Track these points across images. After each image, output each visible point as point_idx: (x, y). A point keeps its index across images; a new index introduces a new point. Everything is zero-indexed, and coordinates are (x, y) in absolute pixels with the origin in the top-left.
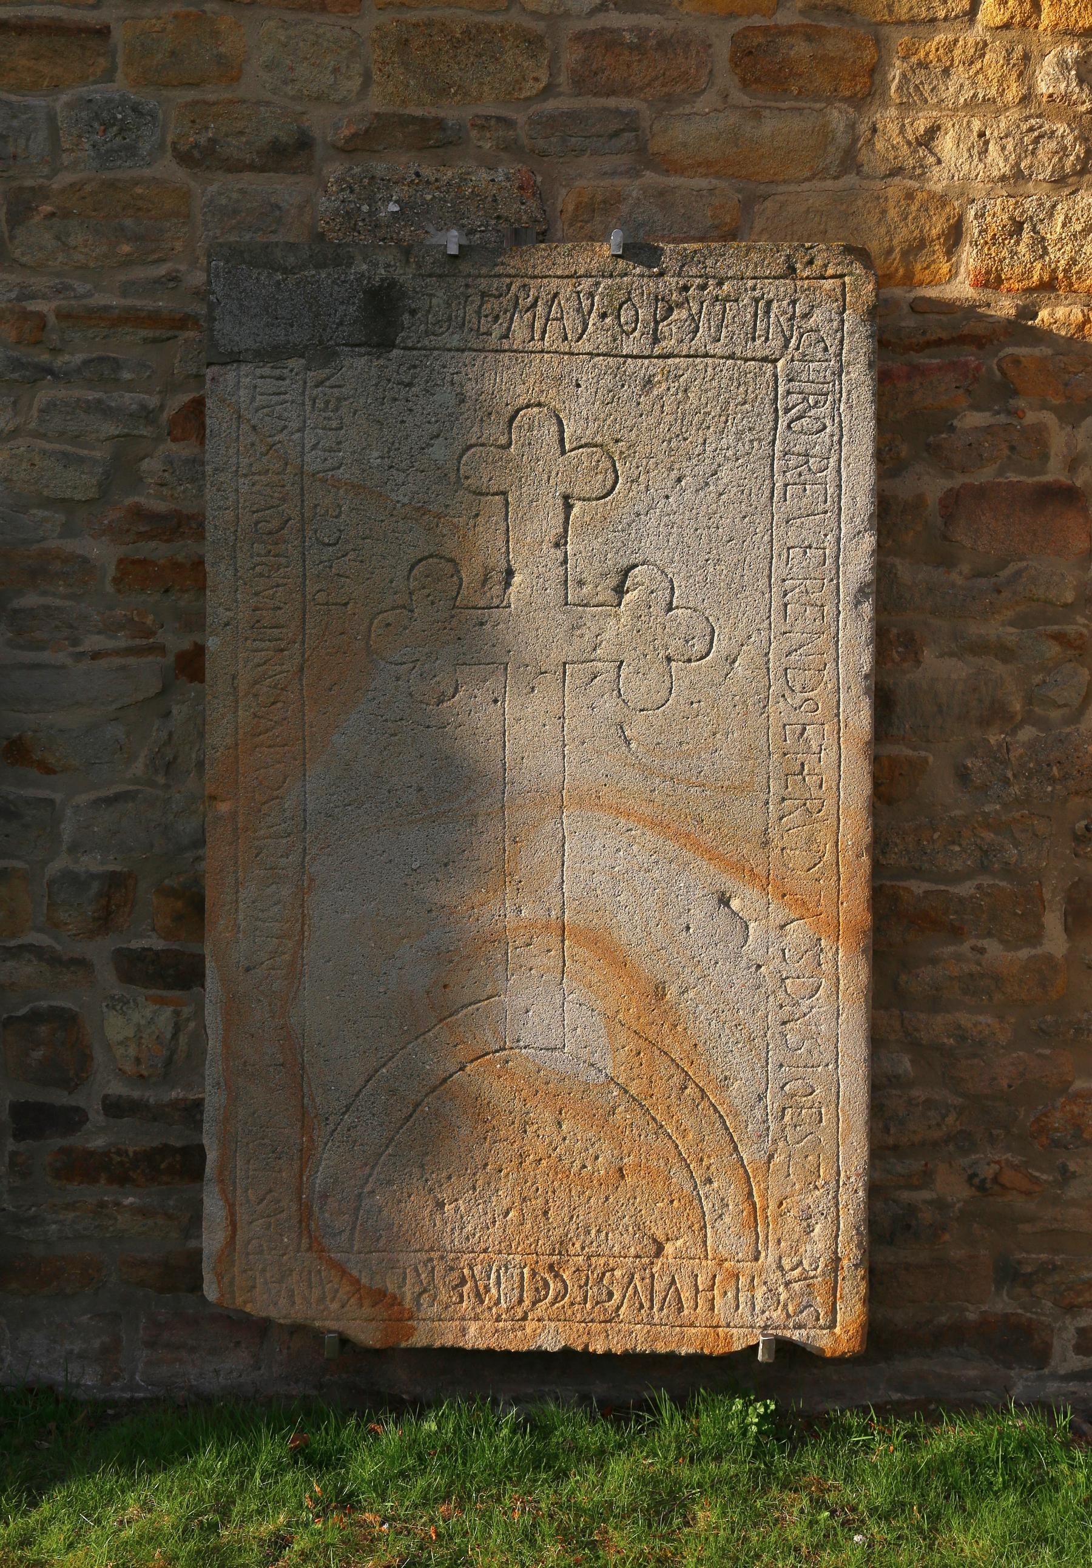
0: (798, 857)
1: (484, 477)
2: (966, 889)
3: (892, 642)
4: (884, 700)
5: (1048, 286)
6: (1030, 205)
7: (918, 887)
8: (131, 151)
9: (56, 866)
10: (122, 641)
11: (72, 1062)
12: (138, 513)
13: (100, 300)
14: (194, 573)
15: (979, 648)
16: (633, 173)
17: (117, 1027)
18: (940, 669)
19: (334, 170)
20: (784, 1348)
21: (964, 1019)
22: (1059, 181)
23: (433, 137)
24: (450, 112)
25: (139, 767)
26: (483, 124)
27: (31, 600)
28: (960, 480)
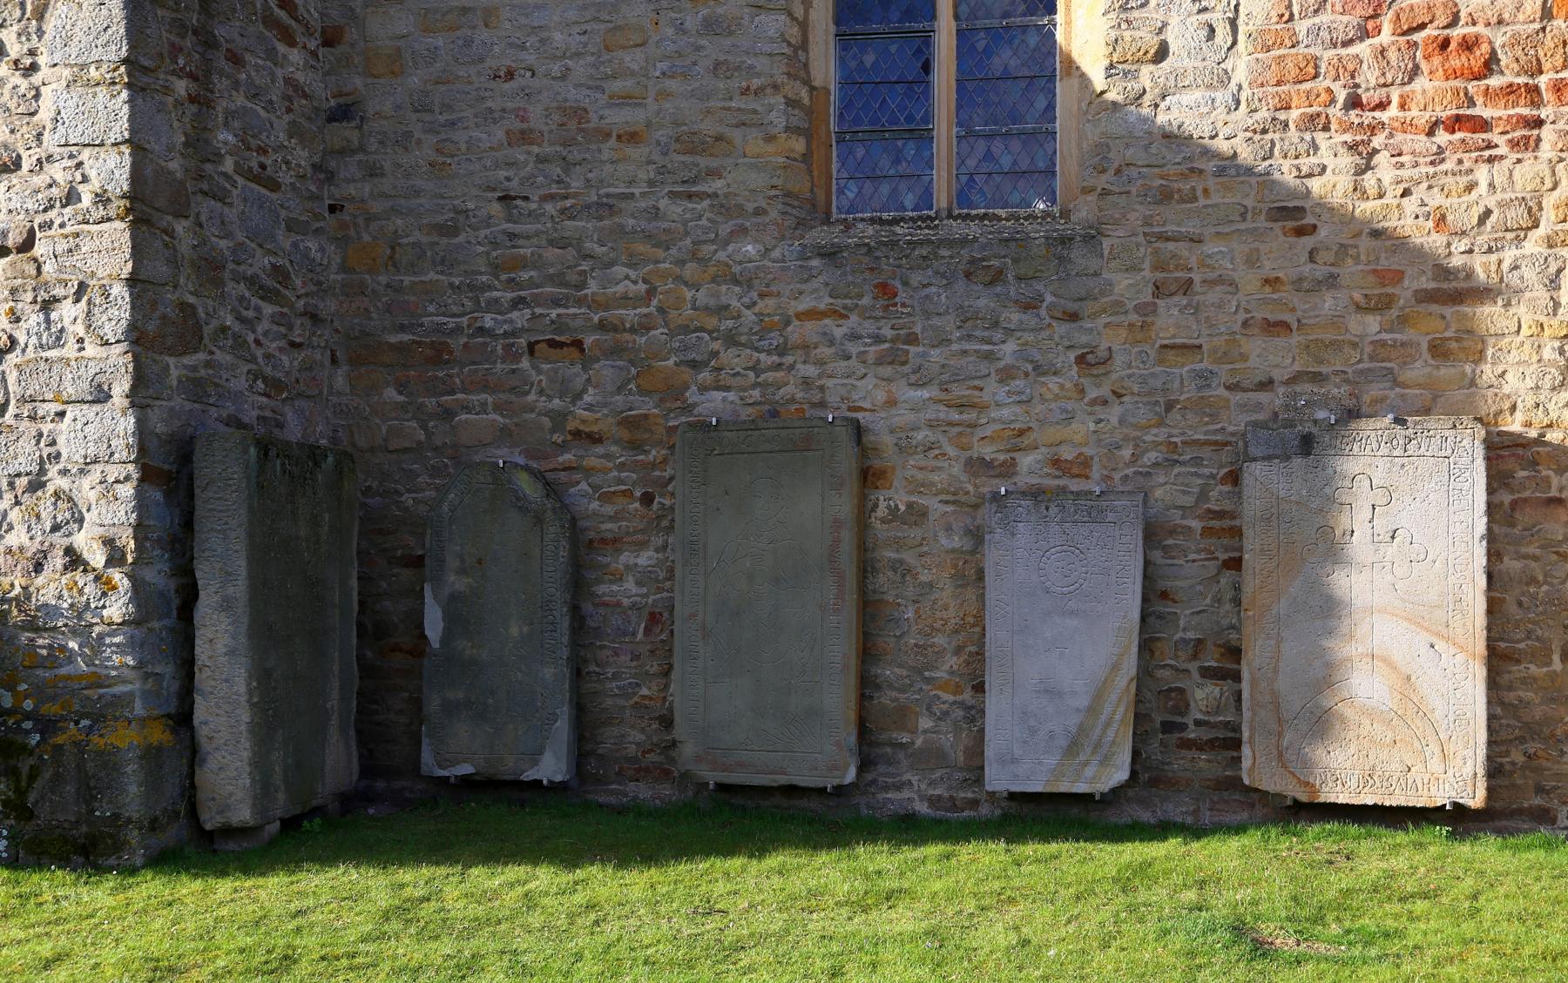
0: (1460, 631)
1: (1344, 499)
2: (1522, 646)
3: (1493, 555)
4: (1490, 577)
5: (1550, 426)
6: (1542, 398)
7: (1503, 645)
8: (1209, 386)
9: (1178, 636)
10: (1203, 556)
11: (1183, 707)
12: (1209, 511)
13: (1197, 437)
14: (1237, 532)
15: (1526, 557)
16: (1392, 389)
17: (1199, 694)
18: (1510, 564)
19: (1281, 390)
20: (1455, 804)
21: (1521, 694)
22: (1554, 389)
23: (1317, 378)
24: (1324, 369)
25: (1208, 601)
26: (1336, 373)
27: (1170, 542)
28: (1517, 496)
